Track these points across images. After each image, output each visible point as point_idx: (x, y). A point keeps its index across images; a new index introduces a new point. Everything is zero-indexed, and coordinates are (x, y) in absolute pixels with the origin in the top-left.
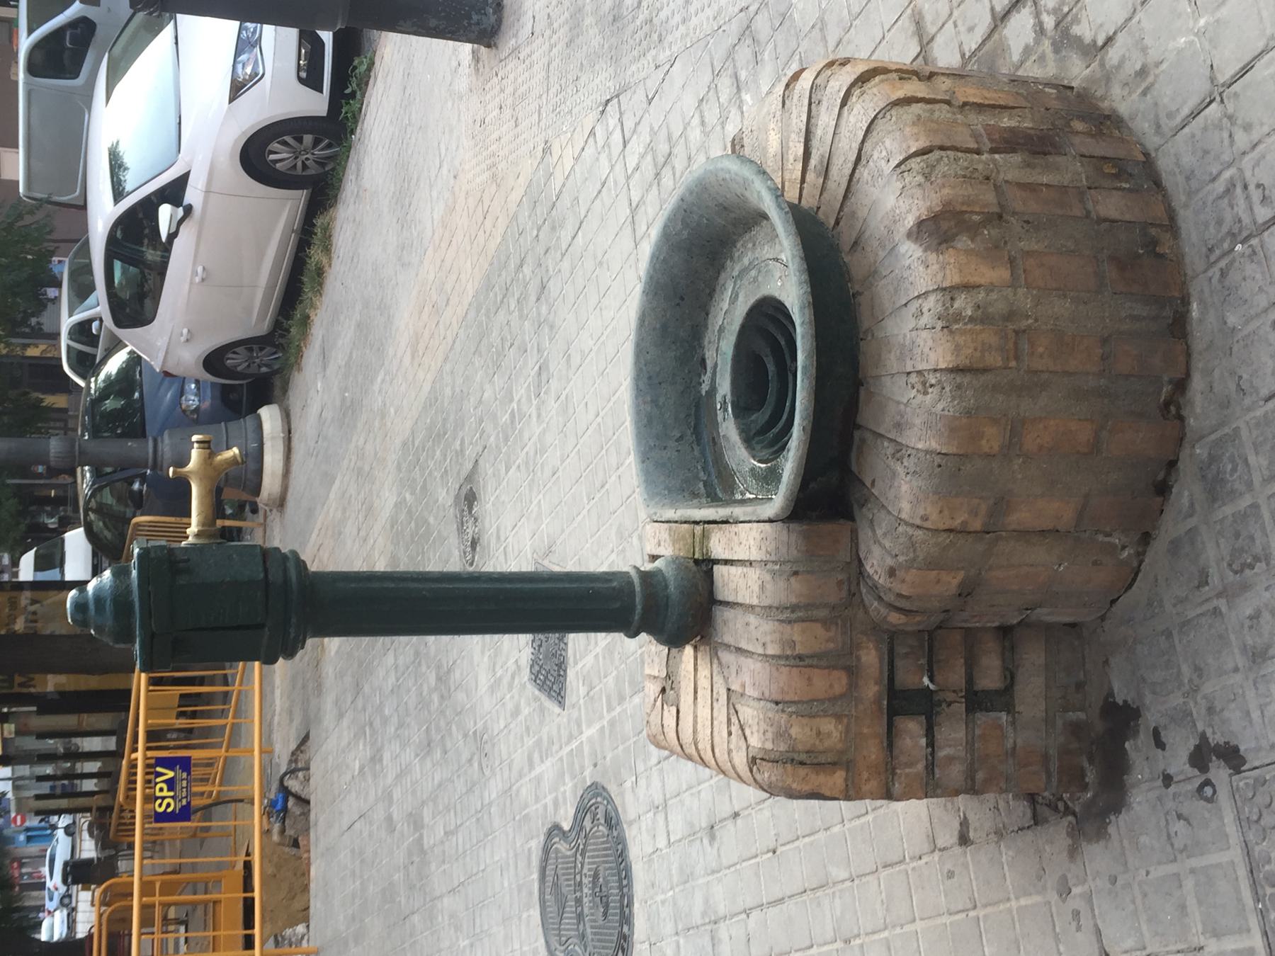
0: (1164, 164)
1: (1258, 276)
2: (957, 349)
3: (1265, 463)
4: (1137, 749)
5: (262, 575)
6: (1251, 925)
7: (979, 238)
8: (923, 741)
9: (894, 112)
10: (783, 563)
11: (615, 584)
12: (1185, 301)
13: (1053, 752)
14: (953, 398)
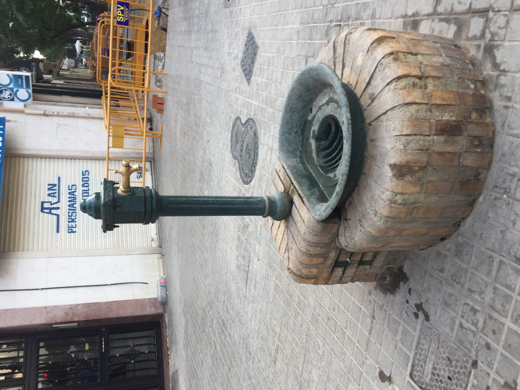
0: (498, 140)
1: (506, 212)
2: (391, 212)
3: (476, 263)
4: (403, 287)
5: (144, 210)
6: (417, 329)
7: (414, 177)
8: (341, 273)
9: (404, 108)
10: (314, 231)
11: (260, 206)
12: (479, 195)
13: (380, 274)
14: (383, 223)
